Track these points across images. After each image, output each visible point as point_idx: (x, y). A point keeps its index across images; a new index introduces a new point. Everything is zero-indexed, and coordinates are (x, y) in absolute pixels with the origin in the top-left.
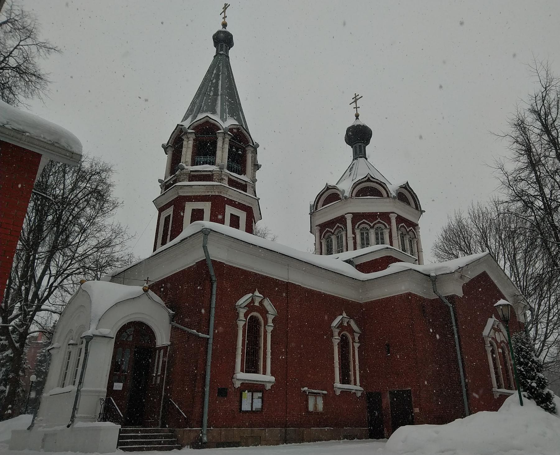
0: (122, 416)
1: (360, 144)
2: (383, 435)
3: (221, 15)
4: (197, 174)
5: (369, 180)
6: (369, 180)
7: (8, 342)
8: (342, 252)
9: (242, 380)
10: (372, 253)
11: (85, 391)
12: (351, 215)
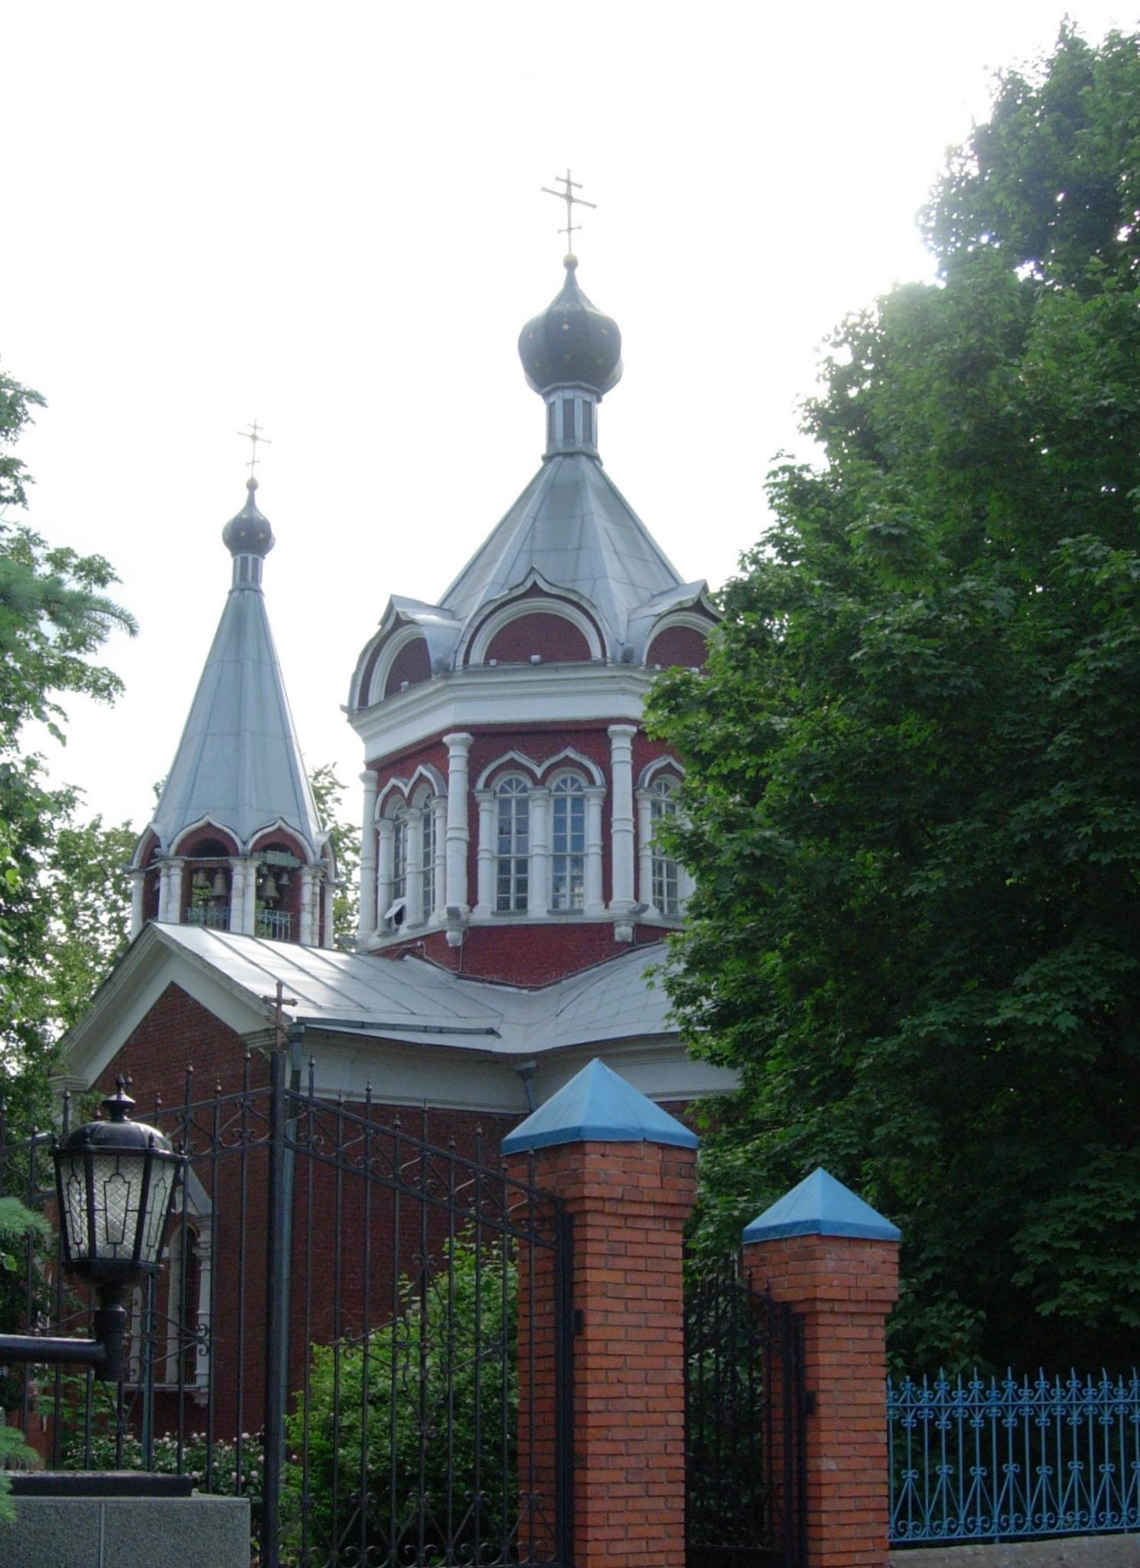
5: (535, 591)
6: (535, 591)
11: (454, 756)
12: (464, 735)
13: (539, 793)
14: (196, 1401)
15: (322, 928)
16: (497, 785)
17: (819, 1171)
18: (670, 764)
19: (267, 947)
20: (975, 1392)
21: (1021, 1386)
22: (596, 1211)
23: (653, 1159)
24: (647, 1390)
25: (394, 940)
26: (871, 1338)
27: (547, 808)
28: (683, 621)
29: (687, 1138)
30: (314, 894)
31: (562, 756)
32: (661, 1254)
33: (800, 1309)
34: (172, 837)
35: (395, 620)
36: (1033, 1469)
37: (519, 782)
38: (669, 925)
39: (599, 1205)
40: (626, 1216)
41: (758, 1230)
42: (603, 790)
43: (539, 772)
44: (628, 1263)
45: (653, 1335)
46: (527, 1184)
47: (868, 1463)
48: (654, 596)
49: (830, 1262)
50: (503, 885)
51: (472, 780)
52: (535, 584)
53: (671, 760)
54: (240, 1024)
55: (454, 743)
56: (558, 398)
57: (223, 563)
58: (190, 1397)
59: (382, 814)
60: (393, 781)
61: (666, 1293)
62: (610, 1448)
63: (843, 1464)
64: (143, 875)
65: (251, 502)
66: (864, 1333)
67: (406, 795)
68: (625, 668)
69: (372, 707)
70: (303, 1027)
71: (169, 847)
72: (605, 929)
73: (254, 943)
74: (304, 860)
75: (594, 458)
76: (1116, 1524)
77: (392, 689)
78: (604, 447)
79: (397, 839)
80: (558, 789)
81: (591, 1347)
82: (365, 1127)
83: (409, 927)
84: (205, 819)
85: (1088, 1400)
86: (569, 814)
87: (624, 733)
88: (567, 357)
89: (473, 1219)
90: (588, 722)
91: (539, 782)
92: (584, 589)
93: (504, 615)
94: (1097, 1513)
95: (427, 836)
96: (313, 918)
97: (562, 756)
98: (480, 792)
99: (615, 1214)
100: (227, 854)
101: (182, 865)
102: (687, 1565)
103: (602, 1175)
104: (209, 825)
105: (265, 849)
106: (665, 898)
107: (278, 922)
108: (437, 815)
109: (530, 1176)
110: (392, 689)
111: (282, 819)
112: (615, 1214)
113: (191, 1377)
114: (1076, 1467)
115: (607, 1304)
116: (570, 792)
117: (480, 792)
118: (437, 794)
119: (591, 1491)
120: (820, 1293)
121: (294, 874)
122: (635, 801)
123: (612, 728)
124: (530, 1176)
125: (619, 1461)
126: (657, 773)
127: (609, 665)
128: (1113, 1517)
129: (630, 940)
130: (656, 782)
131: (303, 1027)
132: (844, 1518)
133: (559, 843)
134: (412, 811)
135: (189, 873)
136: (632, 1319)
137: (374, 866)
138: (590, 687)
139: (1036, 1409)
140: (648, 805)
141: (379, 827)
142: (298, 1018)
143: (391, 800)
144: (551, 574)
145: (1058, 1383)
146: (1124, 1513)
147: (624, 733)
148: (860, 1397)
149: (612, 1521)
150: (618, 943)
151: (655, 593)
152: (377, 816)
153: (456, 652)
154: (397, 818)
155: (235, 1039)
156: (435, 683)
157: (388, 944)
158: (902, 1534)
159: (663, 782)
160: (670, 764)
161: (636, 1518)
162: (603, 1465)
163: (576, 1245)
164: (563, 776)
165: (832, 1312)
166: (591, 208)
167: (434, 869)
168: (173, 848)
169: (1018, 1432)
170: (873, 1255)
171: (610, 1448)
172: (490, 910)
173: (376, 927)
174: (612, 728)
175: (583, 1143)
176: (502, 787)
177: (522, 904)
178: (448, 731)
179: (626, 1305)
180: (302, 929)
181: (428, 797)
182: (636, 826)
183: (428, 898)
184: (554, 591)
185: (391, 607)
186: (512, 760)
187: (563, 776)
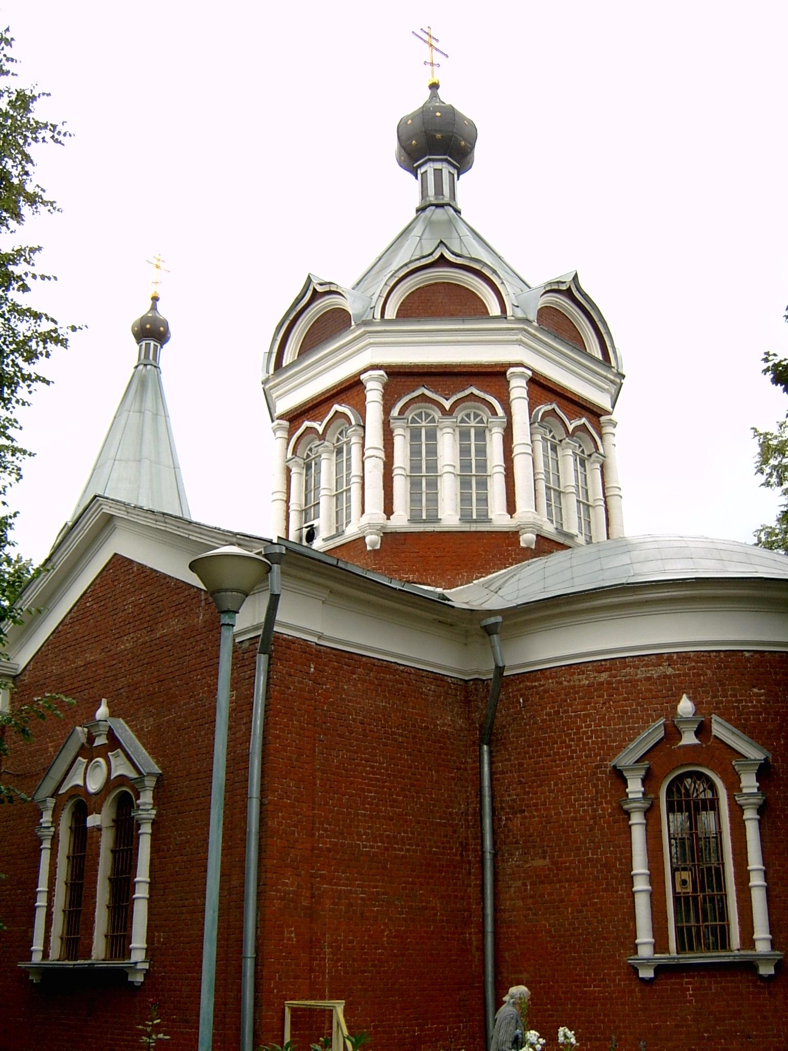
1: (438, 166)
5: (442, 261)
6: (442, 261)
12: (382, 372)
13: (448, 421)
14: (130, 979)
16: (410, 415)
18: (554, 409)
27: (454, 435)
31: (467, 392)
38: (561, 540)
43: (447, 405)
51: (387, 410)
52: (442, 256)
53: (554, 406)
55: (372, 379)
57: (132, 349)
58: (122, 973)
59: (294, 452)
65: (154, 308)
67: (321, 432)
69: (287, 366)
72: (512, 536)
77: (306, 348)
80: (463, 421)
87: (521, 375)
91: (446, 413)
93: (400, 292)
97: (467, 392)
98: (395, 419)
110: (306, 348)
113: (126, 952)
117: (395, 419)
126: (546, 414)
134: (326, 443)
141: (291, 464)
147: (521, 375)
150: (523, 548)
151: (420, 235)
152: (289, 455)
160: (554, 409)
164: (467, 411)
166: (445, 57)
178: (365, 371)
181: (341, 433)
184: (459, 261)
186: (423, 394)
187: (467, 411)
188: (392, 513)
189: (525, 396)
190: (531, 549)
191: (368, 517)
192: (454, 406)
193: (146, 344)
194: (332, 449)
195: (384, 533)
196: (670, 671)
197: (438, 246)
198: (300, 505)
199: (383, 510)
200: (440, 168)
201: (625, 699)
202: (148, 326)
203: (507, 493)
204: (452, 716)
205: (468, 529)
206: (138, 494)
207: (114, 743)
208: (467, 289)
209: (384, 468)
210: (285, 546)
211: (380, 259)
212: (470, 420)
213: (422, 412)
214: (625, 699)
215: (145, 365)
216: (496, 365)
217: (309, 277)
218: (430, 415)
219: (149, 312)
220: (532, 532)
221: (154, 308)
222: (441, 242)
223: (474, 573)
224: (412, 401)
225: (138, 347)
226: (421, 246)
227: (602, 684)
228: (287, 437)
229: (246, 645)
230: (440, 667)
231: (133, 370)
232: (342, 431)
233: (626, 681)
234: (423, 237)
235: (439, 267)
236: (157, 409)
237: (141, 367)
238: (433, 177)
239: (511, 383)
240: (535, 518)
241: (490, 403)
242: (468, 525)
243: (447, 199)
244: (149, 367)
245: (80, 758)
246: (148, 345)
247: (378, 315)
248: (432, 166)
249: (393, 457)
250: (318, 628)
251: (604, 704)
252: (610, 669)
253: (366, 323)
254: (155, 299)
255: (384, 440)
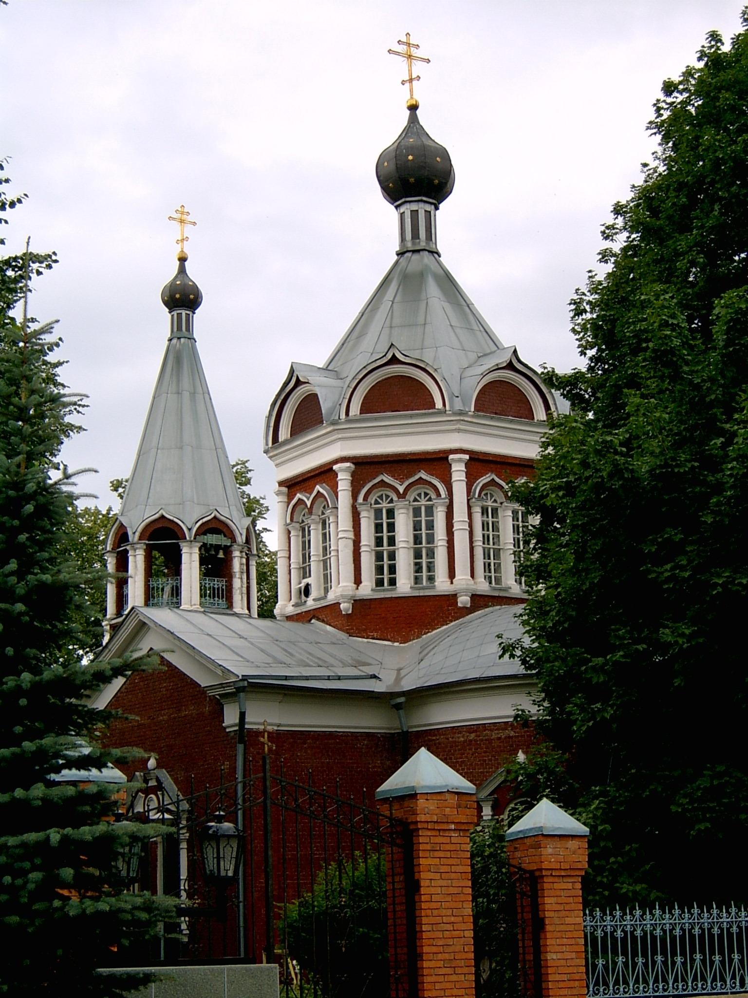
0: (104, 970)
1: (414, 207)
2: (478, 411)
3: (88, 406)
4: (159, 865)
5: (394, 360)
6: (394, 360)
7: (590, 419)
8: (499, 535)
9: (69, 484)
10: (345, 345)
11: (341, 480)
12: (348, 464)
13: (402, 503)
15: (248, 588)
16: (372, 499)
17: (545, 799)
18: (493, 479)
19: (250, 624)
20: (657, 916)
21: (664, 912)
22: (424, 828)
23: (453, 800)
24: (453, 919)
25: (304, 609)
26: (573, 889)
28: (499, 377)
29: (468, 788)
30: (241, 564)
31: (417, 477)
32: (458, 849)
33: (537, 874)
34: (135, 525)
35: (294, 381)
36: (633, 960)
37: (387, 497)
39: (425, 825)
40: (439, 830)
41: (383, 791)
42: (447, 500)
44: (441, 854)
45: (456, 891)
46: (389, 815)
47: (574, 955)
48: (479, 357)
49: (548, 848)
50: (379, 570)
52: (394, 355)
54: (204, 681)
55: (342, 470)
56: (407, 209)
57: (164, 317)
59: (292, 520)
60: (299, 496)
61: (461, 869)
62: (434, 949)
63: (559, 956)
64: (116, 555)
65: (182, 270)
66: (570, 886)
67: (309, 506)
68: (276, 448)
70: (246, 682)
71: (134, 532)
72: (454, 597)
73: (206, 618)
74: (233, 539)
75: (435, 253)
76: (606, 994)
78: (442, 243)
79: (75, 474)
80: (415, 500)
81: (423, 898)
82: (281, 781)
83: (313, 600)
84: (160, 512)
85: (647, 922)
86: (423, 519)
87: (460, 460)
88: (412, 180)
89: (739, 256)
90: (435, 453)
91: (402, 496)
92: (428, 357)
93: (361, 389)
94: (712, 983)
95: (324, 535)
96: (242, 582)
98: (361, 504)
99: (434, 829)
100: (178, 538)
101: (145, 547)
102: (476, 995)
103: (426, 810)
104: (163, 517)
105: (205, 533)
106: (493, 574)
107: (216, 586)
108: (331, 521)
109: (391, 810)
110: (297, 429)
111: (216, 510)
112: (434, 829)
114: (736, 957)
115: (431, 875)
116: (423, 502)
118: (330, 506)
119: (425, 972)
120: (545, 865)
121: (227, 550)
122: (469, 507)
123: (451, 457)
124: (391, 810)
125: (440, 956)
127: (447, 412)
128: (722, 985)
129: (469, 606)
130: (483, 493)
131: (246, 682)
132: (561, 985)
133: (417, 539)
134: (313, 517)
135: (149, 550)
136: (444, 883)
137: (287, 556)
138: (356, 434)
139: (730, 924)
140: (479, 510)
141: (290, 527)
142: (243, 676)
143: (298, 509)
144: (406, 347)
145: (686, 910)
146: (728, 983)
147: (460, 460)
148: (568, 920)
149: (461, 918)
150: (460, 607)
151: (392, 299)
152: (288, 521)
153: (340, 405)
154: (303, 522)
155: (198, 689)
156: (325, 428)
157: (299, 612)
158: (637, 993)
159: (489, 492)
160: (493, 479)
161: (449, 985)
162: (431, 958)
163: (417, 904)
165: (551, 875)
167: (330, 558)
168: (137, 534)
169: (721, 936)
170: (573, 844)
171: (434, 949)
172: (409, 586)
173: (291, 599)
174: (451, 457)
175: (416, 794)
176: (376, 500)
177: (393, 582)
178: (336, 461)
179: (441, 875)
180: (234, 591)
181: (324, 507)
182: (471, 525)
183: (327, 578)
184: (407, 360)
185: (292, 371)
187: (418, 492)
188: (361, 582)
189: (464, 479)
190: (467, 608)
191: (341, 589)
192: (407, 490)
193: (178, 314)
194: (318, 520)
195: (354, 600)
196: (512, 734)
197: (390, 347)
198: (299, 563)
199: (353, 581)
200: (416, 209)
201: (485, 752)
202: (178, 296)
203: (449, 562)
204: (381, 760)
205: (418, 595)
206: (182, 484)
207: (160, 787)
208: (418, 380)
209: (354, 546)
210: (279, 620)
211: (362, 315)
212: (421, 498)
213: (382, 495)
214: (485, 752)
215: (179, 338)
216: (440, 452)
217: (292, 366)
218: (389, 497)
219: (176, 277)
220: (466, 595)
221: (182, 270)
222: (392, 344)
223: (423, 629)
224: (374, 487)
225: (169, 316)
226: (392, 315)
227: (471, 741)
228: (286, 500)
229: (232, 734)
230: (369, 728)
231: (167, 343)
232: (325, 506)
233: (486, 740)
234: (396, 301)
235: (390, 365)
236: (194, 387)
237: (175, 341)
238: (410, 220)
239: (453, 465)
240: (468, 584)
241: (435, 486)
242: (418, 591)
243: (423, 244)
244: (182, 340)
245: (140, 793)
246: (179, 315)
247: (343, 416)
248: (408, 207)
249: (360, 535)
250: (277, 721)
251: (472, 754)
252: (475, 731)
253: (334, 423)
254: (183, 260)
255: (353, 521)
